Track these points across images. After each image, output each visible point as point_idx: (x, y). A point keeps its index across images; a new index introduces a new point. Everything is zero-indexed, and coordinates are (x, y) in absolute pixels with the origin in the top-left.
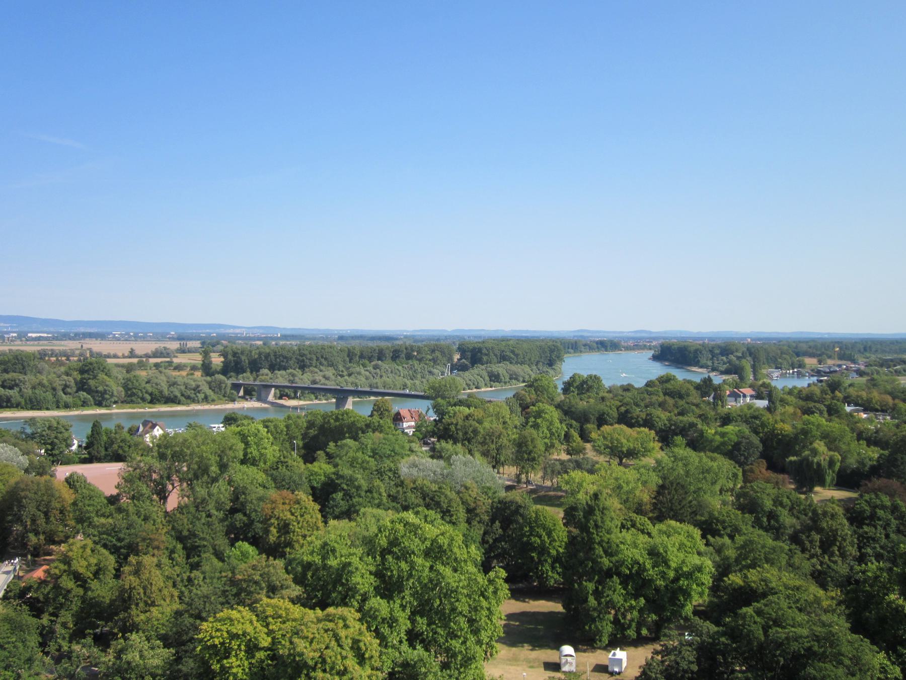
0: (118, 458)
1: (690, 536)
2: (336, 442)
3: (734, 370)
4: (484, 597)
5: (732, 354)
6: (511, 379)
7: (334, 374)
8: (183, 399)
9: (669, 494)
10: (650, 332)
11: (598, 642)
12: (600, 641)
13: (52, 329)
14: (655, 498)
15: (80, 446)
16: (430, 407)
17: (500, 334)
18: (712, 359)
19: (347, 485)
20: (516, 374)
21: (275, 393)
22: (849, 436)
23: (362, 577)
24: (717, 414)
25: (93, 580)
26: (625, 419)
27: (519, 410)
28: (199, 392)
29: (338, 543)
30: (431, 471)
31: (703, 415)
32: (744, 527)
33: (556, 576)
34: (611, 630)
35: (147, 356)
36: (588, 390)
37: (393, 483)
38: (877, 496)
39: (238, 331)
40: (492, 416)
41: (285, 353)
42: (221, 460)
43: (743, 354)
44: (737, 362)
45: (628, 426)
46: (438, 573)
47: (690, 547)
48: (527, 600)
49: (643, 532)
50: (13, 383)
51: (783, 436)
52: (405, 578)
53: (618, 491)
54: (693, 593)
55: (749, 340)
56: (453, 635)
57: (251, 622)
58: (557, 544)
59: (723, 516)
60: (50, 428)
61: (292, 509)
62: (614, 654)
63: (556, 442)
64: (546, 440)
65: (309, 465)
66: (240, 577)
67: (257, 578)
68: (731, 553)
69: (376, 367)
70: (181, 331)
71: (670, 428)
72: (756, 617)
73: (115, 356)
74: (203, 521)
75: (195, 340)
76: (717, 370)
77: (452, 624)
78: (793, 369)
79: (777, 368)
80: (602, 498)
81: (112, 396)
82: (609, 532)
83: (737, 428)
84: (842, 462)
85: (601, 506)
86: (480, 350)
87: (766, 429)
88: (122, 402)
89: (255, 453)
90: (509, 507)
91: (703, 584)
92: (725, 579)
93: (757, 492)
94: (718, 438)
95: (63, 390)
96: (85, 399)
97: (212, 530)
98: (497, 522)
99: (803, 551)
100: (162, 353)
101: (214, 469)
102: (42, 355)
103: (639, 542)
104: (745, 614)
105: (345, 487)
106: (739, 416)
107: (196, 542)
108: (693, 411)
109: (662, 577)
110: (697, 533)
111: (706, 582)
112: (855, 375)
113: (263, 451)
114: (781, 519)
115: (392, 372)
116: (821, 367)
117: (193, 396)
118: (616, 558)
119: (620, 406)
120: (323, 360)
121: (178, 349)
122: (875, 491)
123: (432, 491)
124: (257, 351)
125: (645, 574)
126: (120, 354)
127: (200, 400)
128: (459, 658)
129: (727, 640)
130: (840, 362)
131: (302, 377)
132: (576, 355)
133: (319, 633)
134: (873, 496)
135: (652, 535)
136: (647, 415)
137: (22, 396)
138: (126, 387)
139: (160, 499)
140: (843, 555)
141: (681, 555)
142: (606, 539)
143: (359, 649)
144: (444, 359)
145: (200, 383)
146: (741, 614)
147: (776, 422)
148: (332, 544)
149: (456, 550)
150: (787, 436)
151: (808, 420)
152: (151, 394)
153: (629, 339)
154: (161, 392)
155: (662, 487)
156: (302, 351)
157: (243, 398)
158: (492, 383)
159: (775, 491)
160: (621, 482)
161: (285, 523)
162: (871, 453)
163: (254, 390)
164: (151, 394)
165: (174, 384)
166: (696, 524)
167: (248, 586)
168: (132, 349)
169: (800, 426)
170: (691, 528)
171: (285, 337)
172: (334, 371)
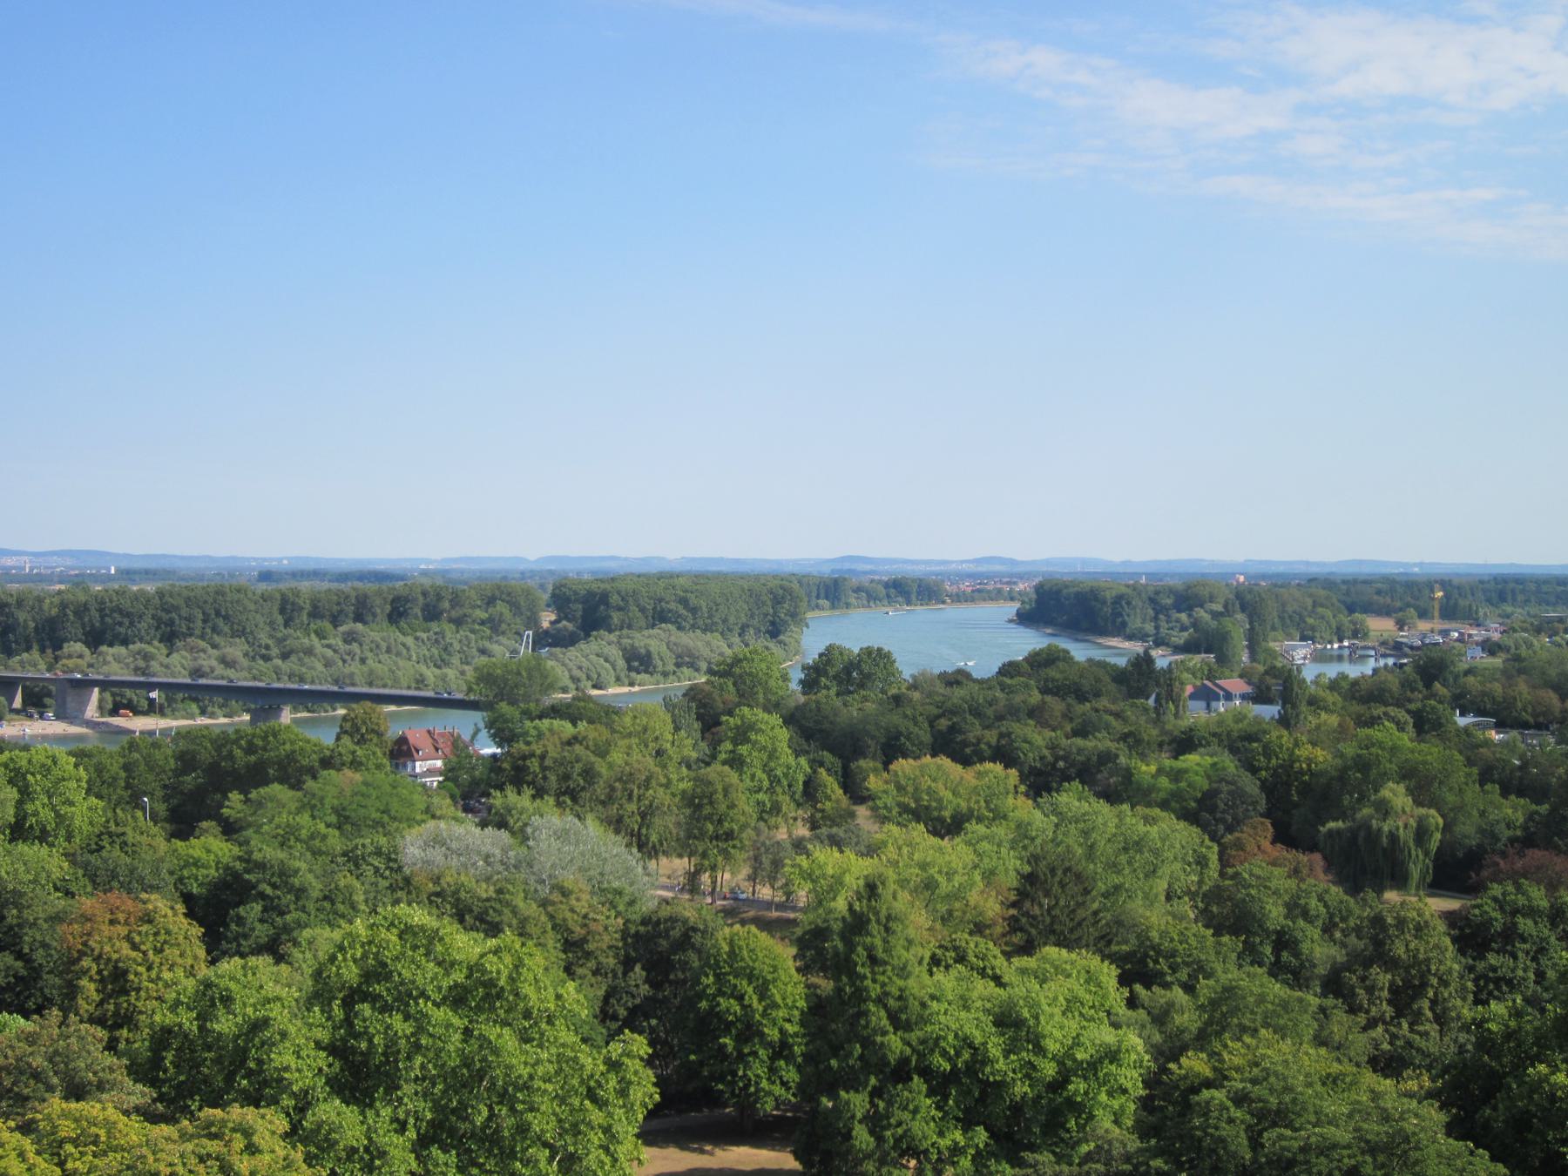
1: (1091, 978)
2: (245, 792)
3: (1209, 642)
5: (1201, 606)
6: (678, 665)
9: (1047, 894)
10: (1013, 562)
14: (1014, 905)
16: (481, 725)
17: (654, 569)
19: (274, 886)
20: (691, 655)
21: (101, 701)
22: (1461, 774)
24: (1163, 732)
26: (950, 744)
27: (697, 725)
29: (238, 981)
30: (479, 853)
31: (1130, 734)
32: (1219, 967)
33: (778, 1090)
36: (862, 686)
37: (386, 883)
38: (1518, 887)
40: (630, 735)
41: (126, 604)
43: (1226, 606)
44: (1214, 624)
46: (484, 1041)
47: (1093, 1007)
48: (708, 1148)
49: (982, 973)
51: (1312, 774)
54: (1098, 1112)
55: (1242, 579)
57: (22, 1155)
58: (782, 1013)
59: (1172, 940)
61: (134, 935)
63: (785, 800)
64: (761, 796)
65: (179, 844)
67: (38, 1061)
68: (1187, 1019)
71: (1054, 765)
72: (1232, 1109)
76: (1167, 645)
78: (1341, 641)
79: (1303, 639)
80: (886, 893)
82: (903, 972)
83: (1209, 760)
84: (1447, 828)
85: (883, 913)
86: (604, 598)
87: (1274, 761)
89: (47, 815)
90: (667, 931)
91: (1125, 1091)
92: (1172, 1066)
93: (1250, 886)
94: (1164, 782)
98: (638, 968)
99: (1353, 1010)
104: (1207, 1103)
105: (269, 891)
106: (1214, 735)
108: (1107, 727)
109: (1027, 1076)
110: (1109, 974)
111: (1129, 1085)
112: (1478, 652)
113: (63, 810)
114: (1305, 947)
115: (388, 651)
116: (1404, 636)
118: (919, 1034)
119: (938, 717)
120: (220, 622)
122: (1515, 877)
124: (56, 600)
125: (988, 1069)
129: (1166, 1163)
130: (1447, 626)
131: (166, 661)
132: (837, 613)
133: (184, 1164)
134: (1510, 888)
135: (1006, 979)
136: (1001, 735)
140: (1441, 1020)
141: (1073, 1025)
144: (518, 620)
146: (1198, 1104)
147: (1296, 744)
148: (223, 983)
149: (527, 989)
150: (1321, 773)
151: (1368, 737)
155: (1030, 879)
156: (168, 599)
157: (23, 712)
158: (633, 674)
159: (1292, 884)
160: (933, 871)
161: (116, 967)
162: (1510, 811)
163: (49, 695)
166: (1113, 958)
169: (1349, 749)
170: (1094, 962)
171: (127, 574)
172: (246, 647)
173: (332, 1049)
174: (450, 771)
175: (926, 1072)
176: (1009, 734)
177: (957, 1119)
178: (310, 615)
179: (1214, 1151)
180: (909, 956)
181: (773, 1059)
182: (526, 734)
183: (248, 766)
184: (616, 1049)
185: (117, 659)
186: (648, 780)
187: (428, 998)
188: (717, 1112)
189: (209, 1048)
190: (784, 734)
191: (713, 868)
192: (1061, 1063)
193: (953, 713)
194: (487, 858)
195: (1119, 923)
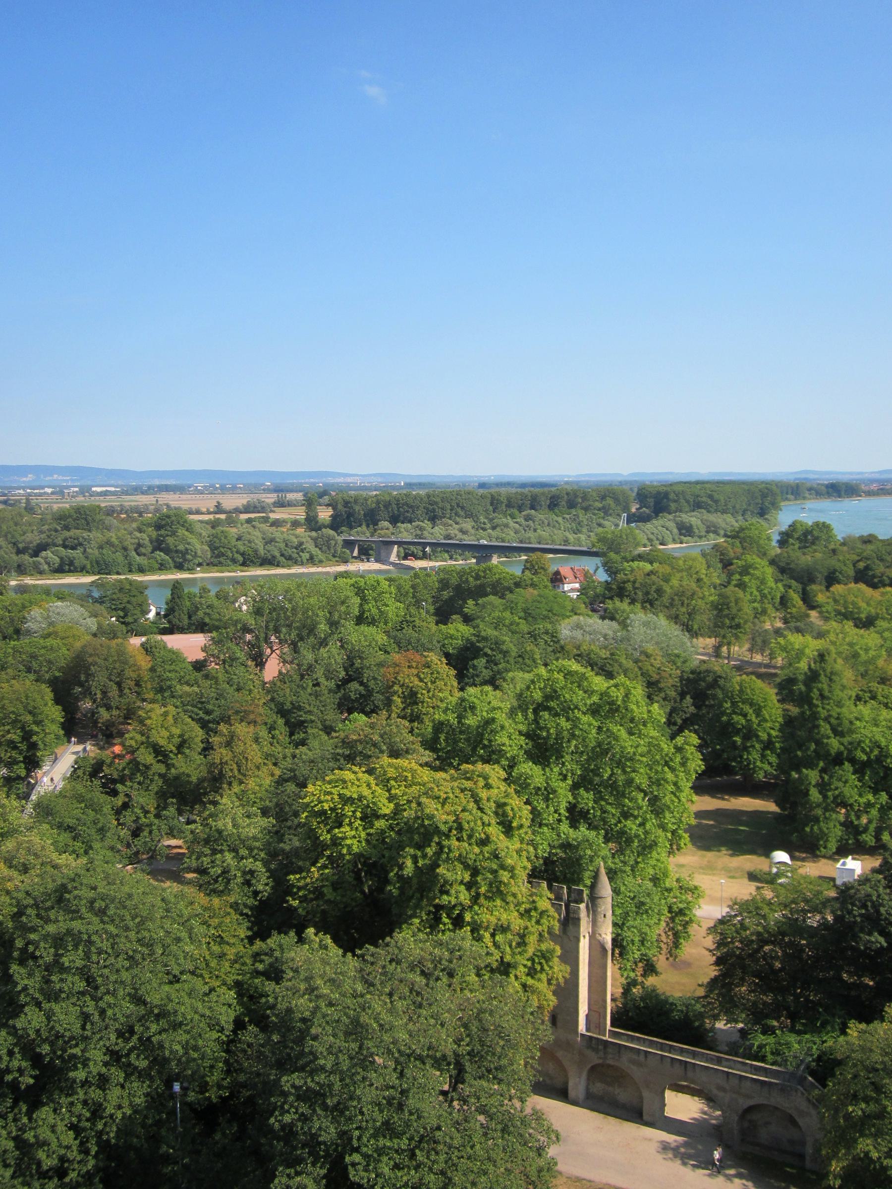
0: (201, 628)
4: (669, 768)
6: (708, 532)
7: (473, 527)
8: (282, 559)
11: (822, 849)
12: (825, 848)
13: (120, 483)
15: (158, 614)
16: (600, 565)
19: (492, 649)
20: (715, 527)
21: (398, 552)
23: (510, 738)
26: (864, 576)
27: (720, 565)
30: (601, 633)
33: (767, 767)
34: (840, 833)
35: (238, 511)
36: (813, 543)
37: (551, 649)
39: (349, 480)
41: (410, 501)
45: (868, 585)
50: (76, 541)
52: (566, 740)
53: (853, 660)
56: (626, 815)
60: (121, 590)
62: (844, 864)
63: (769, 607)
64: (756, 605)
66: (355, 738)
67: (376, 738)
69: (528, 518)
70: (278, 481)
73: (198, 512)
74: (309, 690)
75: (296, 491)
77: (627, 800)
82: (839, 704)
85: (829, 670)
86: (666, 495)
88: (208, 565)
89: (374, 611)
95: (136, 550)
96: (162, 560)
97: (321, 702)
98: (688, 697)
100: (255, 507)
101: (323, 627)
102: (110, 512)
105: (489, 652)
107: (301, 716)
113: (383, 608)
115: (549, 525)
119: (859, 561)
120: (459, 510)
121: (275, 502)
123: (602, 658)
126: (204, 510)
127: (305, 561)
132: (798, 502)
137: (87, 558)
138: (213, 547)
139: (256, 665)
142: (834, 714)
143: (505, 814)
144: (618, 508)
145: (304, 540)
152: (243, 554)
153: (872, 481)
154: (256, 551)
158: (682, 537)
160: (857, 648)
161: (411, 690)
163: (372, 549)
164: (243, 554)
165: (272, 540)
167: (364, 748)
168: (218, 502)
171: (409, 485)
174: (584, 589)
175: (853, 761)
177: (870, 787)
178: (506, 506)
181: (764, 749)
182: (624, 570)
183: (476, 586)
186: (693, 594)
187: (579, 710)
190: (769, 571)
191: (729, 644)
193: (867, 559)
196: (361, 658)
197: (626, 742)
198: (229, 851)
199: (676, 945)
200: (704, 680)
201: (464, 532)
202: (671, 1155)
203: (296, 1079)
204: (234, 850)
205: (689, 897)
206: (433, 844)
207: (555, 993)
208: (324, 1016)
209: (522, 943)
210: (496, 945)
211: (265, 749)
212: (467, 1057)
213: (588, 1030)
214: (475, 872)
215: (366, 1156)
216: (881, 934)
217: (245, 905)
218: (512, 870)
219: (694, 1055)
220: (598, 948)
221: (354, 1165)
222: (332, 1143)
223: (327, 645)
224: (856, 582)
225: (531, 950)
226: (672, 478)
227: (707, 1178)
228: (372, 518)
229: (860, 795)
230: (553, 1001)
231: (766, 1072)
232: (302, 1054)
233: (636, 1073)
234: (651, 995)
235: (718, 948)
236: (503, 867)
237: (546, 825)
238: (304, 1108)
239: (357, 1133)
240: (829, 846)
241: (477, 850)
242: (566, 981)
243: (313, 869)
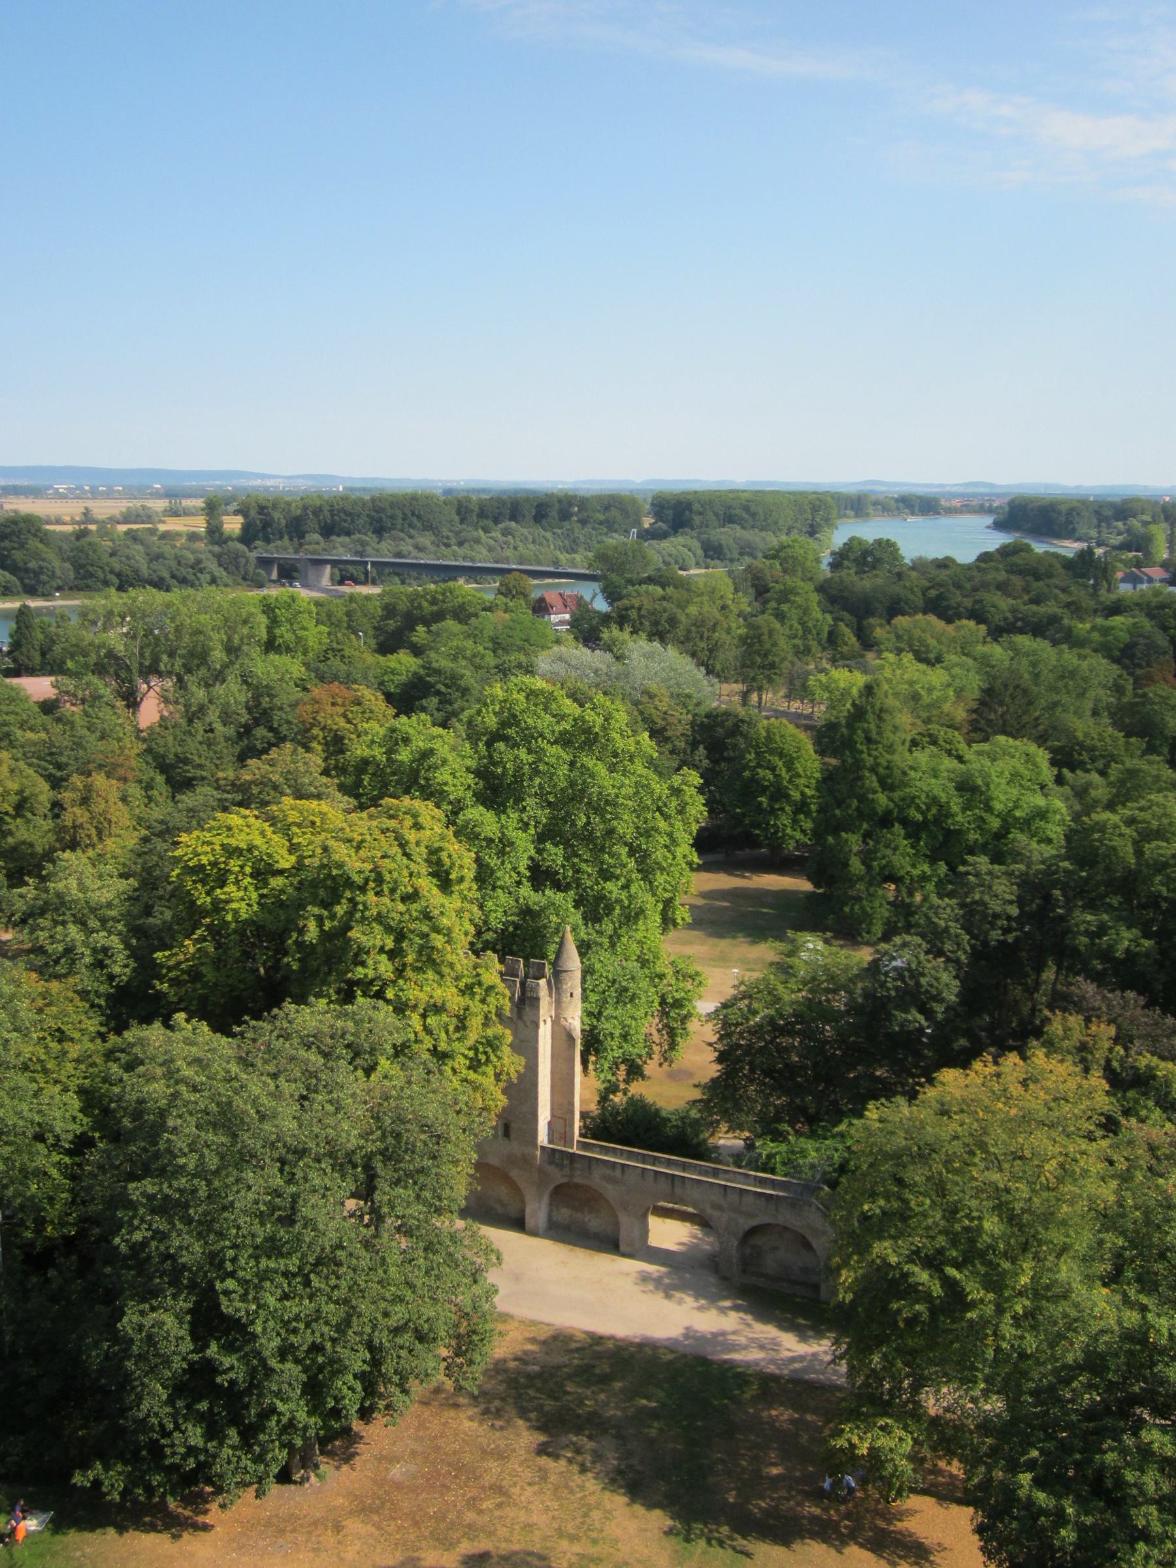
4: (662, 814)
6: (741, 554)
10: (991, 485)
18: (1099, 526)
19: (447, 686)
23: (453, 775)
25: (14, 818)
26: (939, 607)
27: (751, 591)
28: (201, 571)
30: (590, 668)
31: (1073, 603)
33: (798, 835)
34: (887, 914)
35: (114, 520)
36: (874, 567)
39: (269, 483)
42: (229, 639)
44: (1142, 530)
49: (949, 753)
58: (802, 781)
63: (813, 644)
64: (796, 641)
65: (381, 658)
66: (248, 778)
67: (275, 778)
70: (171, 483)
74: (200, 738)
75: (196, 496)
80: (879, 693)
81: (53, 576)
82: (890, 749)
83: (1131, 620)
85: (878, 707)
88: (71, 589)
89: (289, 637)
94: (1096, 636)
98: (701, 747)
100: (138, 516)
103: (942, 767)
105: (443, 689)
108: (1056, 598)
109: (979, 827)
110: (1042, 757)
111: (1053, 836)
113: (300, 633)
115: (534, 542)
117: (191, 577)
120: (415, 520)
126: (68, 519)
128: (617, 911)
135: (967, 757)
136: (976, 602)
138: (78, 567)
141: (1015, 792)
143: (439, 863)
145: (203, 556)
148: (404, 728)
152: (119, 575)
153: (954, 495)
154: (137, 572)
155: (989, 692)
160: (917, 687)
164: (119, 575)
165: (159, 557)
170: (1032, 748)
173: (478, 773)
175: (905, 822)
176: (981, 601)
177: (926, 856)
179: (1108, 856)
180: (896, 738)
181: (795, 813)
184: (676, 780)
185: (343, 546)
186: (715, 625)
187: (544, 738)
188: (756, 852)
189: (394, 774)
190: (815, 597)
191: (760, 689)
192: (1004, 820)
193: (940, 585)
194: (596, 672)
195: (1054, 728)
196: (271, 696)
197: (604, 780)
198: (74, 923)
199: (673, 1046)
200: (722, 725)
201: (419, 548)
202: (651, 1287)
203: (149, 1186)
204: (82, 923)
205: (688, 985)
206: (344, 901)
207: (505, 1091)
208: (187, 1103)
209: (462, 1027)
210: (428, 1030)
211: (137, 811)
212: (379, 1157)
213: (550, 1142)
214: (400, 937)
215: (243, 1282)
216: (920, 1012)
217: (97, 994)
218: (448, 934)
219: (684, 1167)
220: (563, 1036)
221: (227, 1293)
222: (200, 1269)
223: (224, 681)
224: (925, 613)
225: (473, 1037)
226: (697, 487)
227: (695, 1312)
228: (296, 528)
229: (914, 866)
230: (502, 1101)
231: (773, 1184)
232: (157, 1155)
233: (611, 1192)
234: (638, 1107)
235: (721, 1039)
236: (437, 930)
237: (502, 888)
238: (160, 1224)
239: (230, 1253)
240: (873, 929)
241: (401, 907)
242: (520, 1076)
243: (187, 942)
